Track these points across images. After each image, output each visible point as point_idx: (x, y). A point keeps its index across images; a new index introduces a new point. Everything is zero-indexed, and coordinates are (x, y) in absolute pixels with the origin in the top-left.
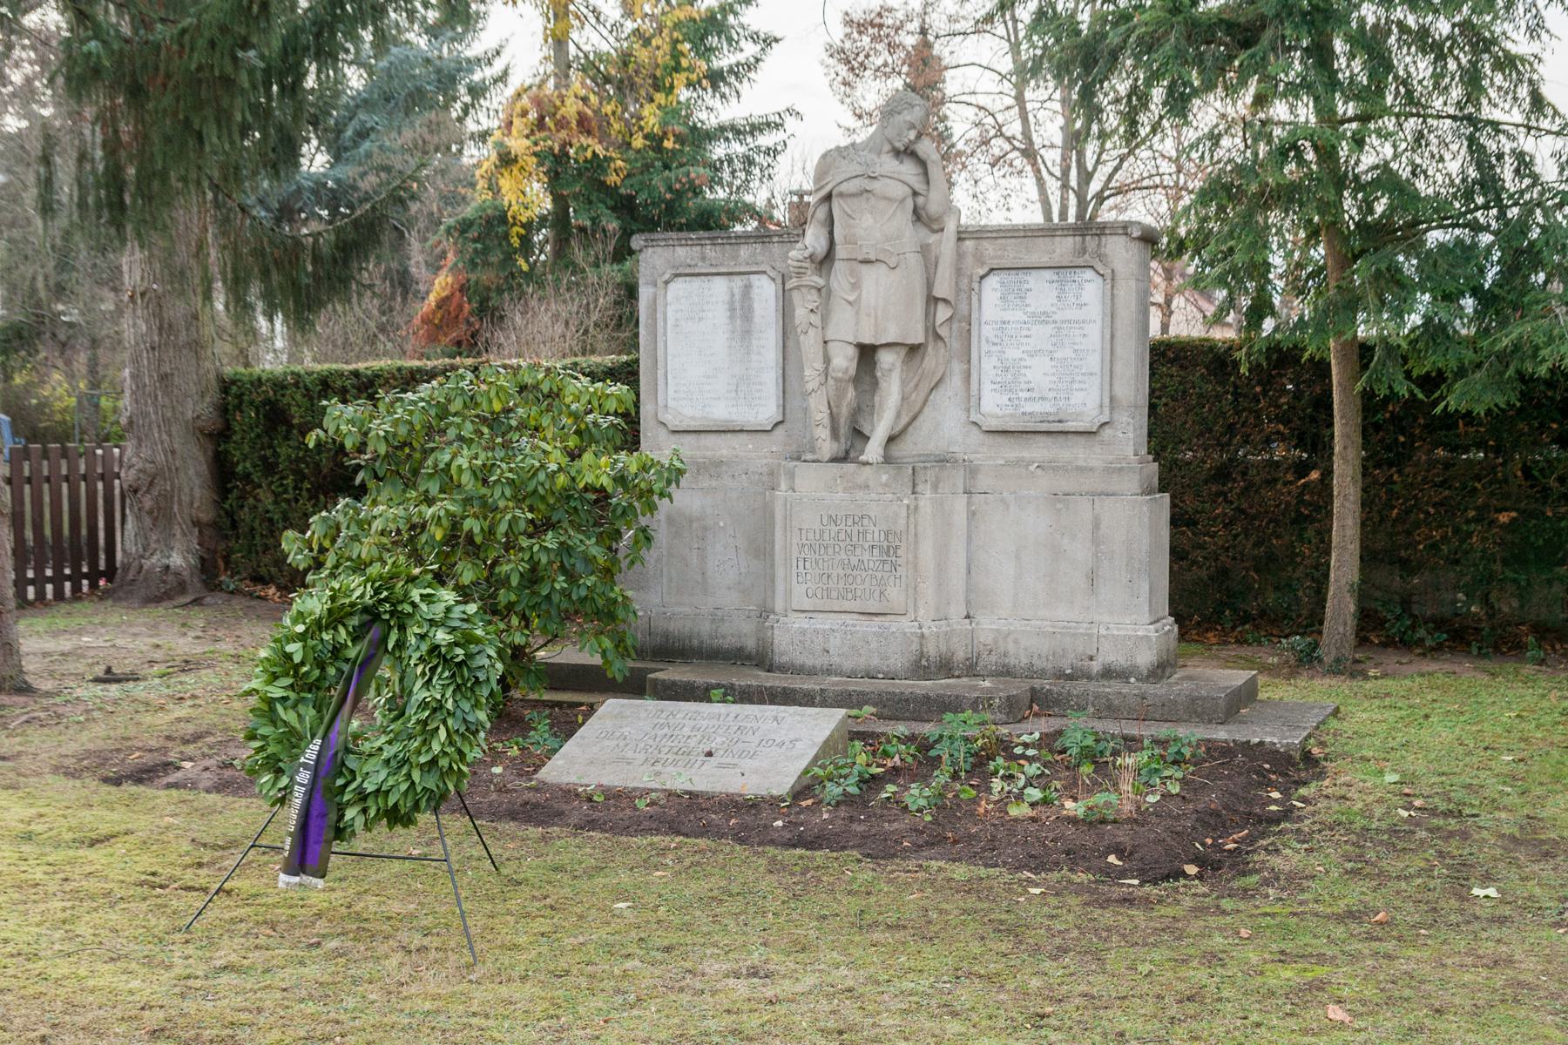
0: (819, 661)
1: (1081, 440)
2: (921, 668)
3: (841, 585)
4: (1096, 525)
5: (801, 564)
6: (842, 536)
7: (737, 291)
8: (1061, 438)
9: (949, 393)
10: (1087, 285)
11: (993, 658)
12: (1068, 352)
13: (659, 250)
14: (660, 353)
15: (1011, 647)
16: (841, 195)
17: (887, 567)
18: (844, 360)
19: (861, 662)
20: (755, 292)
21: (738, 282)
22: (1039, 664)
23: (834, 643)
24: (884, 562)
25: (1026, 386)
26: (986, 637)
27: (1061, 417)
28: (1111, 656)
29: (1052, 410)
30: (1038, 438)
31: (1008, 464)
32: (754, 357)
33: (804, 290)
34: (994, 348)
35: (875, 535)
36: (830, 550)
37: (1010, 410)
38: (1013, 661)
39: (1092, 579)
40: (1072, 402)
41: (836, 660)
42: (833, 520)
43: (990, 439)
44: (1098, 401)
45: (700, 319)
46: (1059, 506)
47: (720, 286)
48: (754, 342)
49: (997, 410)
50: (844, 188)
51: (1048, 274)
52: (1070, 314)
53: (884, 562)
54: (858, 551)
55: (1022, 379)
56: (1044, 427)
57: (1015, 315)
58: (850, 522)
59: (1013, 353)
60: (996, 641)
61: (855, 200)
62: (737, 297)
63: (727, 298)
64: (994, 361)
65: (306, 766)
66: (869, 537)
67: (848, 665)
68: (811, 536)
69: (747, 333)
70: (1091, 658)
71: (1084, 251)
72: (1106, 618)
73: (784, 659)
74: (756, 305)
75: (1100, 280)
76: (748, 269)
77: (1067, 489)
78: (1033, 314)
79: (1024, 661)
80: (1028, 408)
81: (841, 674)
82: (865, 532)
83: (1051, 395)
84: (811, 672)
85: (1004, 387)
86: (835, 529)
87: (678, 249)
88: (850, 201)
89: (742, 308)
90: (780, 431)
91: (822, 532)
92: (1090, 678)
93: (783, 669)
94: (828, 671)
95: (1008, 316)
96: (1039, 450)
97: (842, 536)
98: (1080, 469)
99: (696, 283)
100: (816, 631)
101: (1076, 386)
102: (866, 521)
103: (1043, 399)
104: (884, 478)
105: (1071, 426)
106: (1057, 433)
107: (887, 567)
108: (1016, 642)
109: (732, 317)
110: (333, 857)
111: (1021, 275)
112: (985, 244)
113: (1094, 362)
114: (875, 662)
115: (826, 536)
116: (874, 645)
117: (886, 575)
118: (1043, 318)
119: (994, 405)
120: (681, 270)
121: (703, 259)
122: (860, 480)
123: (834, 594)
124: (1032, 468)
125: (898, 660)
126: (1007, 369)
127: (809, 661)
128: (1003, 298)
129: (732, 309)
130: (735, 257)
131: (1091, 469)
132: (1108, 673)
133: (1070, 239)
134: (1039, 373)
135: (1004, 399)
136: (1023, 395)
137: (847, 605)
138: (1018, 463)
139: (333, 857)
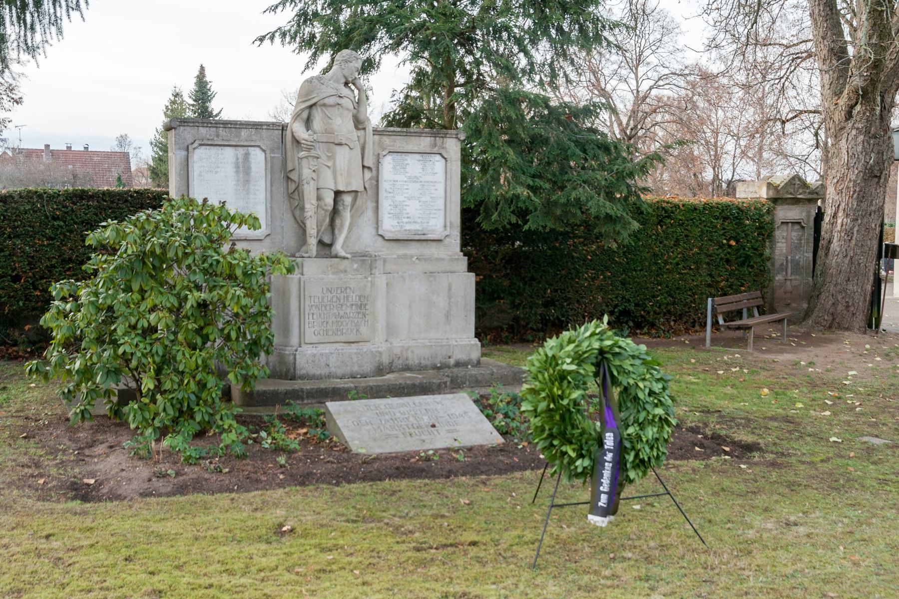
0: (324, 371)
1: (434, 244)
2: (380, 370)
3: (334, 327)
4: (450, 289)
5: (311, 317)
6: (335, 299)
7: (240, 156)
8: (424, 243)
9: (366, 219)
10: (437, 163)
11: (400, 362)
12: (427, 198)
13: (188, 129)
14: (269, 195)
15: (410, 355)
16: (324, 105)
17: (360, 316)
18: (329, 199)
19: (348, 370)
20: (252, 158)
21: (241, 151)
22: (424, 362)
23: (332, 360)
24: (359, 313)
25: (406, 216)
26: (397, 351)
27: (425, 232)
28: (460, 356)
29: (420, 228)
30: (413, 243)
31: (399, 257)
32: (251, 196)
33: (310, 159)
34: (390, 195)
35: (353, 298)
36: (328, 308)
37: (398, 228)
38: (410, 362)
39: (448, 315)
40: (430, 224)
41: (333, 370)
42: (330, 291)
43: (387, 244)
44: (443, 223)
45: (217, 172)
46: (431, 279)
47: (229, 152)
48: (252, 187)
49: (392, 229)
50: (326, 101)
51: (417, 156)
52: (428, 178)
53: (359, 313)
54: (344, 308)
55: (404, 212)
56: (417, 237)
57: (401, 177)
58: (339, 291)
59: (399, 198)
60: (402, 353)
61: (332, 109)
62: (240, 160)
63: (234, 160)
64: (390, 202)
65: (610, 451)
66: (350, 299)
67: (340, 372)
68: (317, 300)
69: (247, 182)
70: (449, 357)
71: (435, 145)
72: (454, 336)
73: (303, 372)
74: (253, 165)
75: (443, 161)
76: (245, 144)
77: (432, 270)
78: (410, 177)
79: (417, 362)
80: (408, 227)
81: (337, 378)
82: (348, 297)
83: (419, 220)
84: (319, 378)
85: (396, 216)
86: (330, 295)
87: (201, 129)
88: (329, 109)
89: (244, 167)
90: (268, 240)
91: (323, 298)
92: (449, 367)
93: (302, 377)
94: (329, 376)
95: (397, 177)
96: (413, 250)
97: (335, 299)
98: (438, 259)
99: (214, 150)
100: (322, 355)
101: (432, 216)
102: (348, 291)
103: (415, 222)
104: (355, 266)
105: (430, 237)
106: (423, 240)
107: (360, 316)
108: (412, 352)
109: (237, 172)
110: (621, 501)
111: (404, 156)
112: (385, 138)
113: (441, 203)
114: (356, 369)
115: (325, 300)
116: (355, 360)
117: (360, 320)
118: (415, 179)
119: (389, 225)
120: (205, 142)
121: (218, 136)
122: (342, 267)
123: (330, 333)
124: (414, 259)
125: (368, 367)
126: (396, 206)
127: (318, 372)
128: (394, 168)
129: (237, 167)
130: (239, 136)
131: (443, 259)
132: (458, 364)
133: (429, 139)
134: (413, 208)
135: (395, 222)
136: (405, 220)
137: (338, 338)
138: (405, 256)
139: (621, 501)
